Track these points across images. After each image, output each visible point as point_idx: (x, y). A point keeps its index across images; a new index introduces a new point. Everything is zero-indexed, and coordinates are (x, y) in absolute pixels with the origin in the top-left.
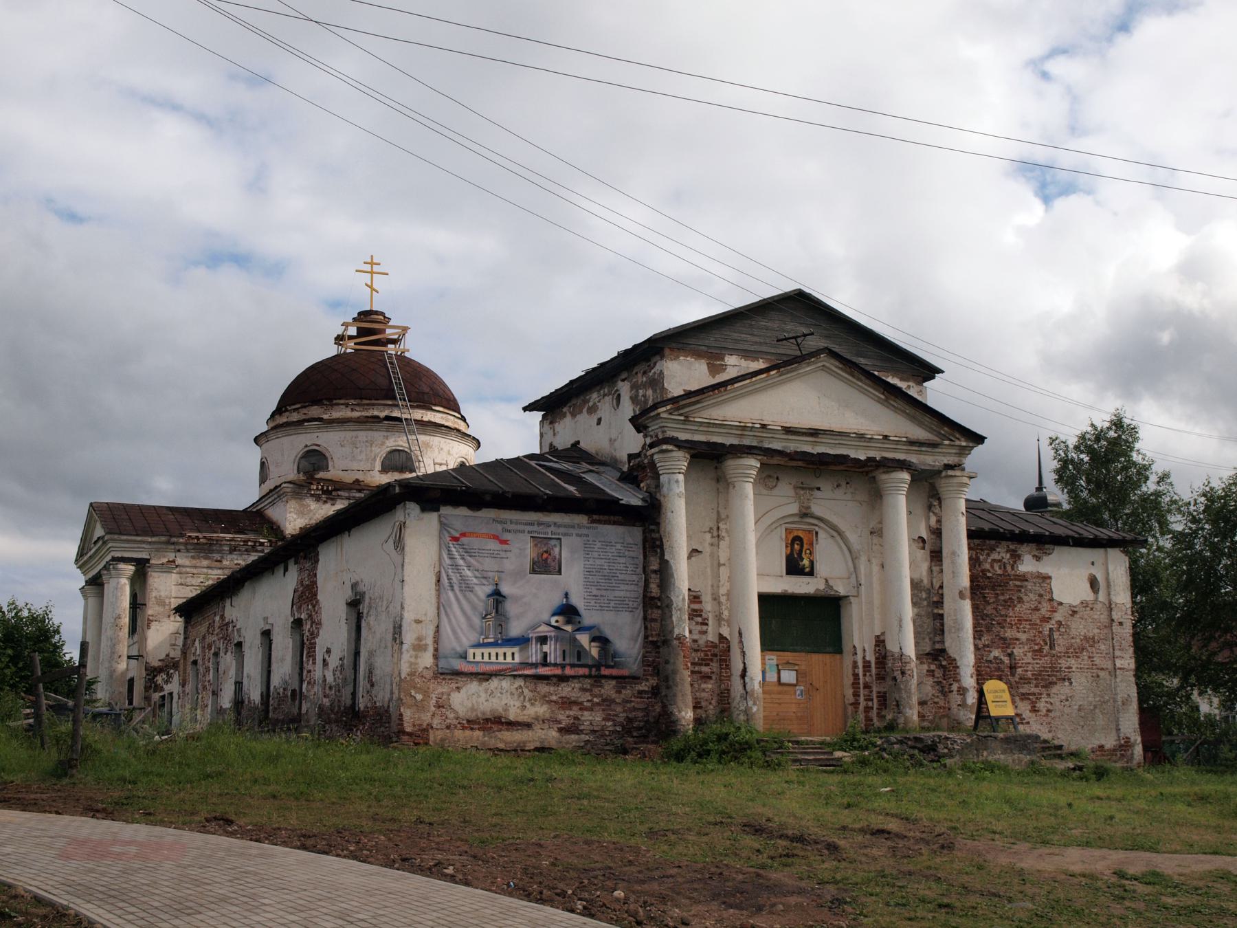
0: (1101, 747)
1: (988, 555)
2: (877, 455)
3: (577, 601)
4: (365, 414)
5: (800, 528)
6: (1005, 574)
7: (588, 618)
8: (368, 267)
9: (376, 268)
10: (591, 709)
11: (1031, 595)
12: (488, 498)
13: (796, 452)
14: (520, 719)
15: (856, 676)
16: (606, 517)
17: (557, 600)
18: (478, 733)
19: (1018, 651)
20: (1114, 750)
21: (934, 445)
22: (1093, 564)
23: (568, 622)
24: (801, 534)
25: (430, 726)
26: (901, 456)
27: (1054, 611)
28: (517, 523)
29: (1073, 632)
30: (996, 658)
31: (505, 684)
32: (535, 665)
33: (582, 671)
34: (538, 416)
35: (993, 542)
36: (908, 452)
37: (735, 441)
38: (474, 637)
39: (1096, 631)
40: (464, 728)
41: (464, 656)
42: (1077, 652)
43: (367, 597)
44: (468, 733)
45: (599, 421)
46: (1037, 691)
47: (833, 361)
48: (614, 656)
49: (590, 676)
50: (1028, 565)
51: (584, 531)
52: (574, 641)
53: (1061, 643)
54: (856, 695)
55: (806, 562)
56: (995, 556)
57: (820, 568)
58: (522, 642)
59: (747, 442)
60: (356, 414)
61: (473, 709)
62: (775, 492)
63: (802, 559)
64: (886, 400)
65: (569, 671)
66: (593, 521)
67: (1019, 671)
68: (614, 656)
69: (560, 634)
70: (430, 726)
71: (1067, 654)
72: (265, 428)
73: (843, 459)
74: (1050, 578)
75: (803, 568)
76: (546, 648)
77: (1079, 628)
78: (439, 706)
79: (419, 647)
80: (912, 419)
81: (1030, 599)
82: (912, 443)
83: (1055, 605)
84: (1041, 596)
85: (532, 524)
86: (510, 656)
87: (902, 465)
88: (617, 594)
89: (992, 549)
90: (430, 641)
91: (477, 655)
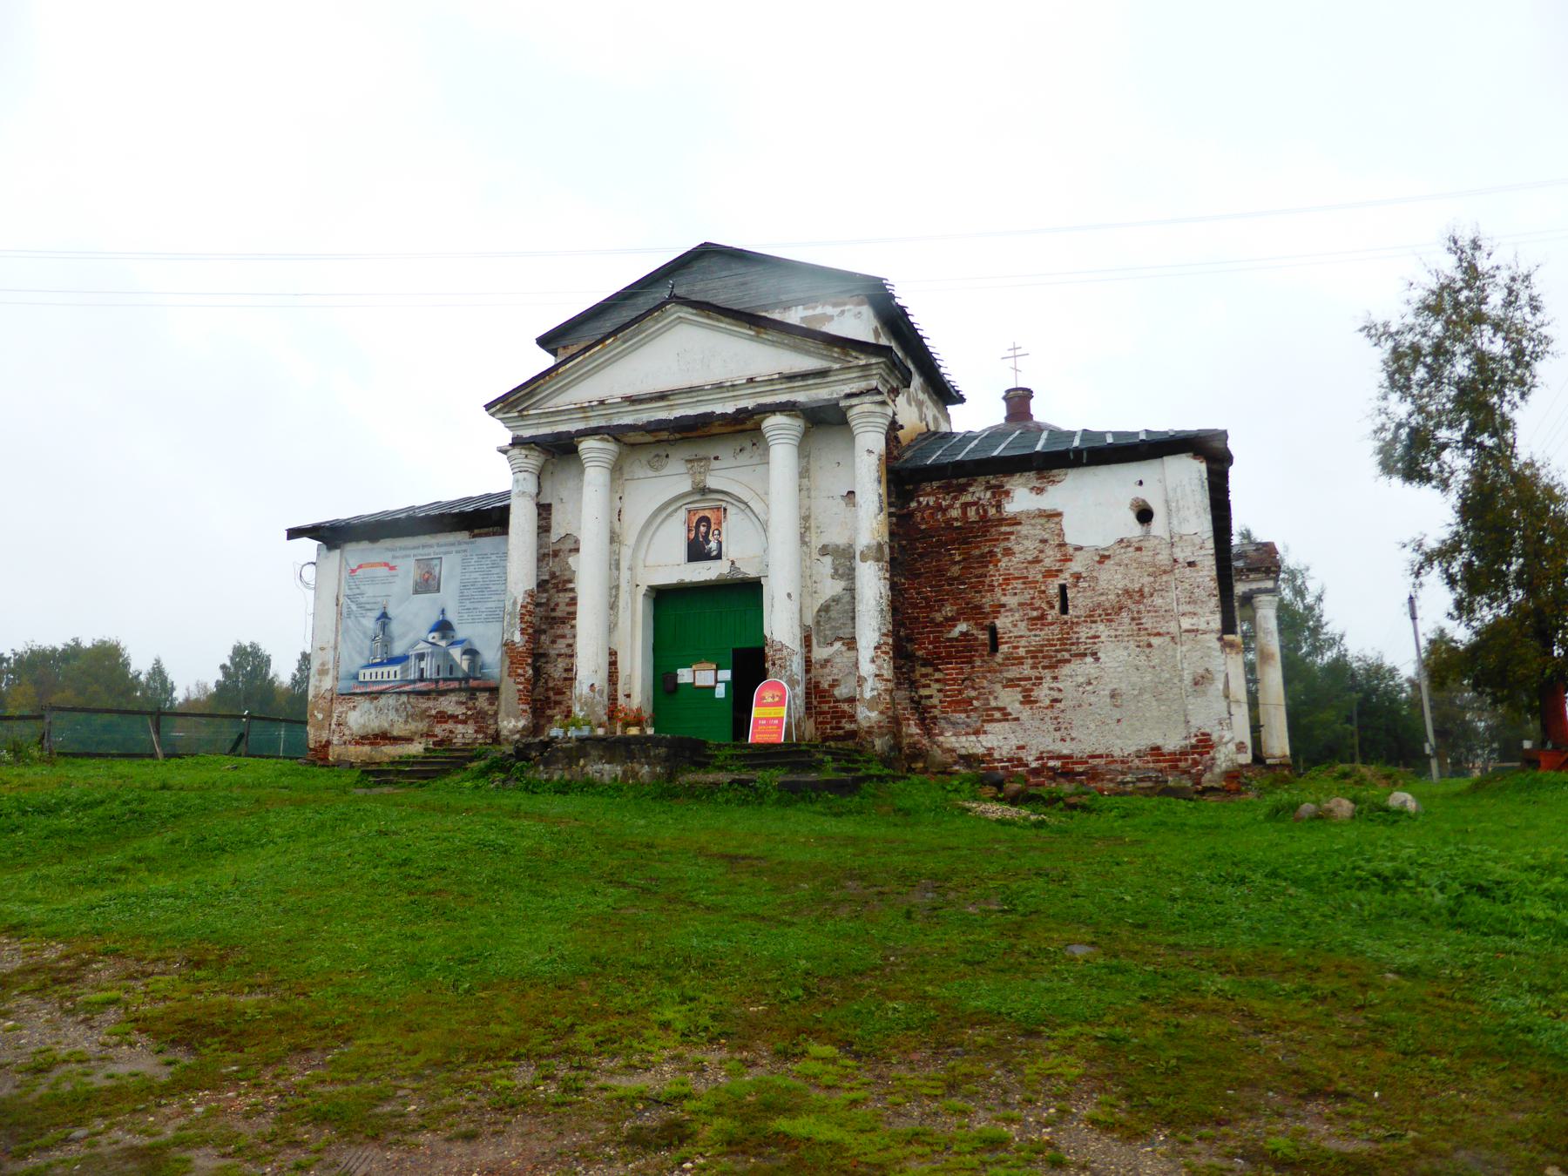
0: (1156, 750)
2: (750, 403)
3: (451, 616)
5: (704, 506)
6: (984, 518)
7: (461, 632)
8: (1011, 353)
9: (1018, 352)
10: (464, 722)
11: (1027, 543)
13: (650, 423)
17: (435, 617)
18: (367, 749)
19: (1002, 623)
20: (1184, 753)
21: (823, 373)
22: (1141, 483)
23: (443, 638)
24: (707, 514)
27: (1067, 559)
28: (406, 548)
29: (1103, 584)
30: (962, 634)
31: (392, 701)
32: (414, 682)
33: (455, 685)
35: (963, 481)
37: (581, 426)
39: (1146, 580)
41: (356, 677)
42: (1110, 614)
46: (1034, 673)
47: (685, 309)
51: (464, 547)
52: (447, 655)
53: (1079, 601)
56: (967, 498)
57: (730, 551)
58: (402, 659)
63: (708, 542)
65: (442, 686)
67: (1004, 648)
69: (436, 650)
70: (328, 743)
71: (1091, 618)
73: (706, 419)
75: (710, 551)
76: (423, 665)
77: (1112, 580)
79: (323, 672)
82: (791, 378)
84: (1044, 541)
89: (963, 489)
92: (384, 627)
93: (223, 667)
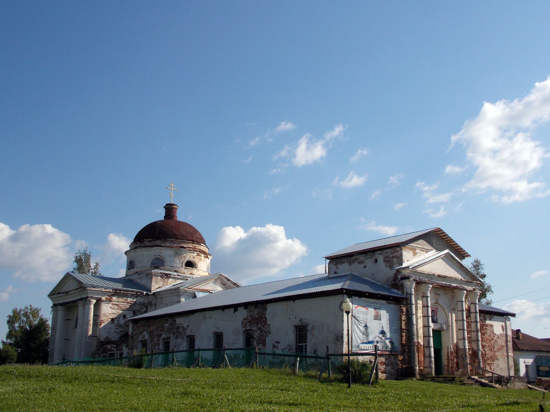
15: (448, 356)
17: (381, 329)
19: (486, 349)
23: (383, 336)
34: (328, 261)
38: (359, 342)
41: (358, 347)
43: (310, 326)
45: (365, 267)
52: (385, 342)
54: (448, 362)
66: (388, 303)
72: (129, 249)
91: (362, 346)
92: (366, 329)
93: (484, 276)
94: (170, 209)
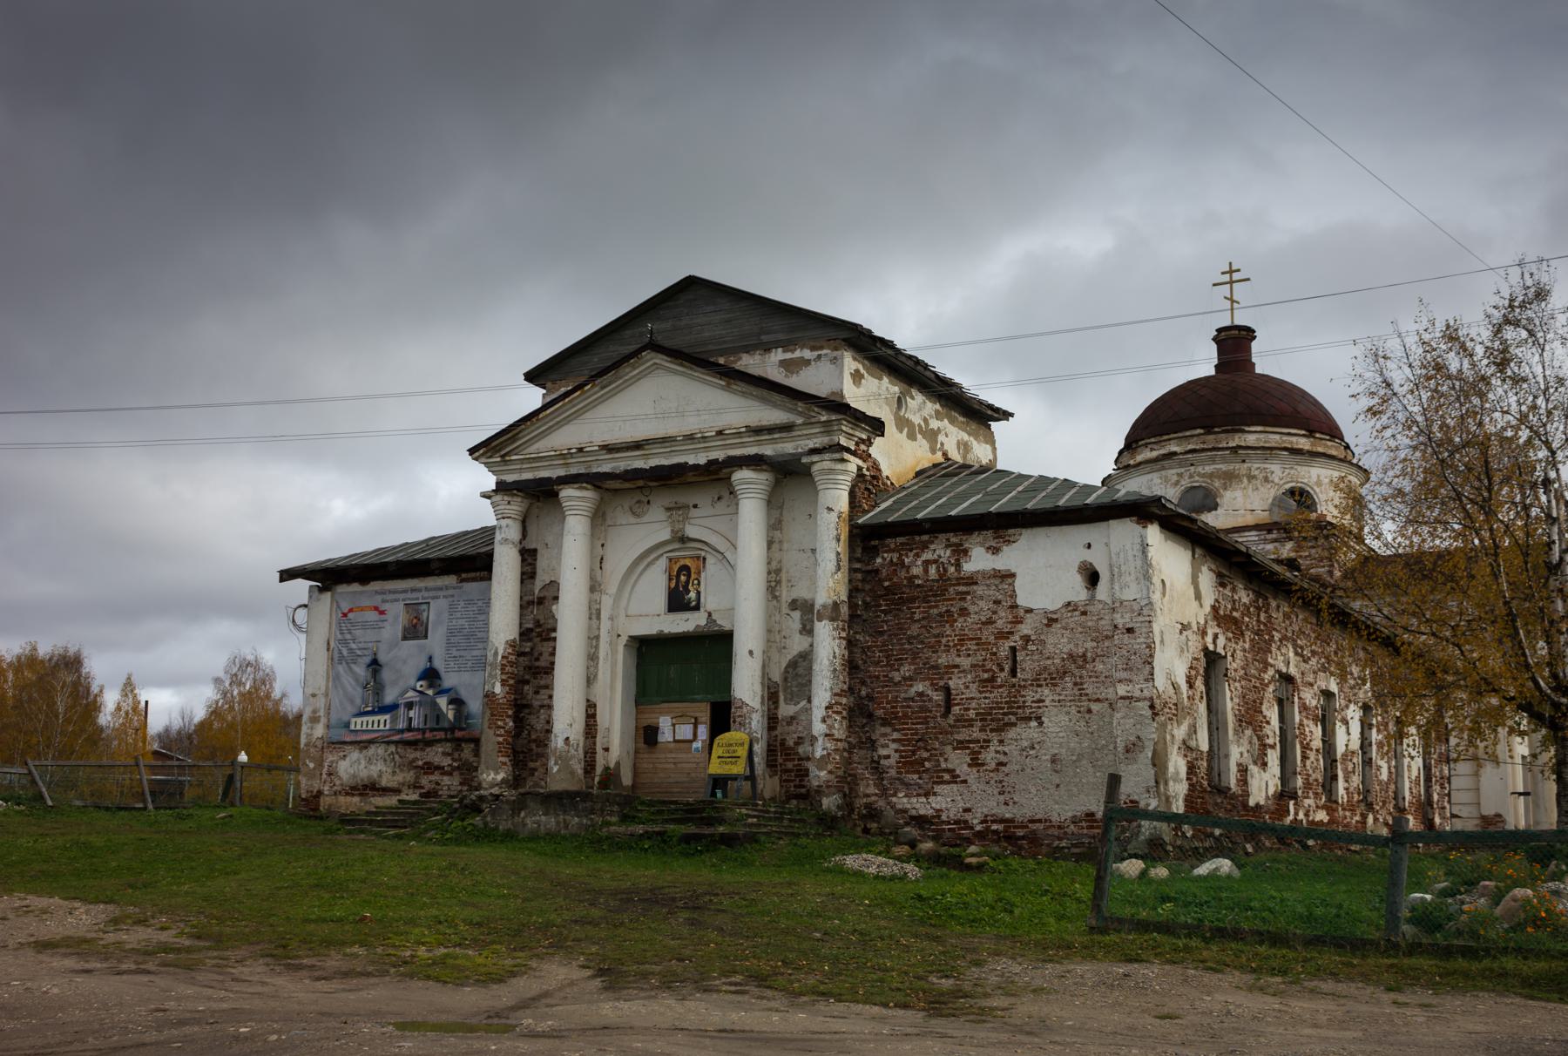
1: (917, 555)
2: (720, 455)
3: (438, 664)
4: (1162, 452)
6: (943, 575)
7: (449, 680)
8: (1226, 278)
9: (1236, 276)
10: (450, 774)
11: (982, 604)
12: (434, 565)
14: (390, 785)
16: (472, 575)
17: (422, 664)
18: (356, 799)
21: (787, 428)
22: (1089, 546)
23: (430, 686)
24: (688, 562)
25: (320, 793)
26: (752, 451)
27: (1018, 621)
28: (395, 592)
29: (1050, 648)
30: (921, 694)
32: (402, 731)
33: (441, 735)
35: (925, 538)
36: (759, 443)
37: (561, 472)
38: (351, 709)
39: (1089, 645)
40: (347, 794)
41: (347, 725)
42: (1053, 678)
44: (349, 799)
46: (982, 736)
48: (467, 717)
49: (447, 740)
50: (979, 560)
52: (435, 705)
53: (1028, 665)
55: (692, 595)
56: (927, 556)
58: (392, 708)
59: (573, 471)
60: (1155, 454)
61: (354, 776)
62: (645, 519)
64: (728, 385)
66: (462, 581)
67: (956, 710)
68: (467, 717)
70: (320, 793)
71: (1037, 682)
73: (682, 468)
74: (1013, 575)
76: (412, 714)
77: (1059, 643)
78: (330, 774)
80: (763, 400)
81: (980, 608)
82: (758, 431)
83: (1018, 614)
84: (997, 602)
85: (405, 591)
86: (382, 722)
87: (755, 462)
88: (475, 653)
90: (322, 713)
91: (358, 723)
94: (1234, 343)
